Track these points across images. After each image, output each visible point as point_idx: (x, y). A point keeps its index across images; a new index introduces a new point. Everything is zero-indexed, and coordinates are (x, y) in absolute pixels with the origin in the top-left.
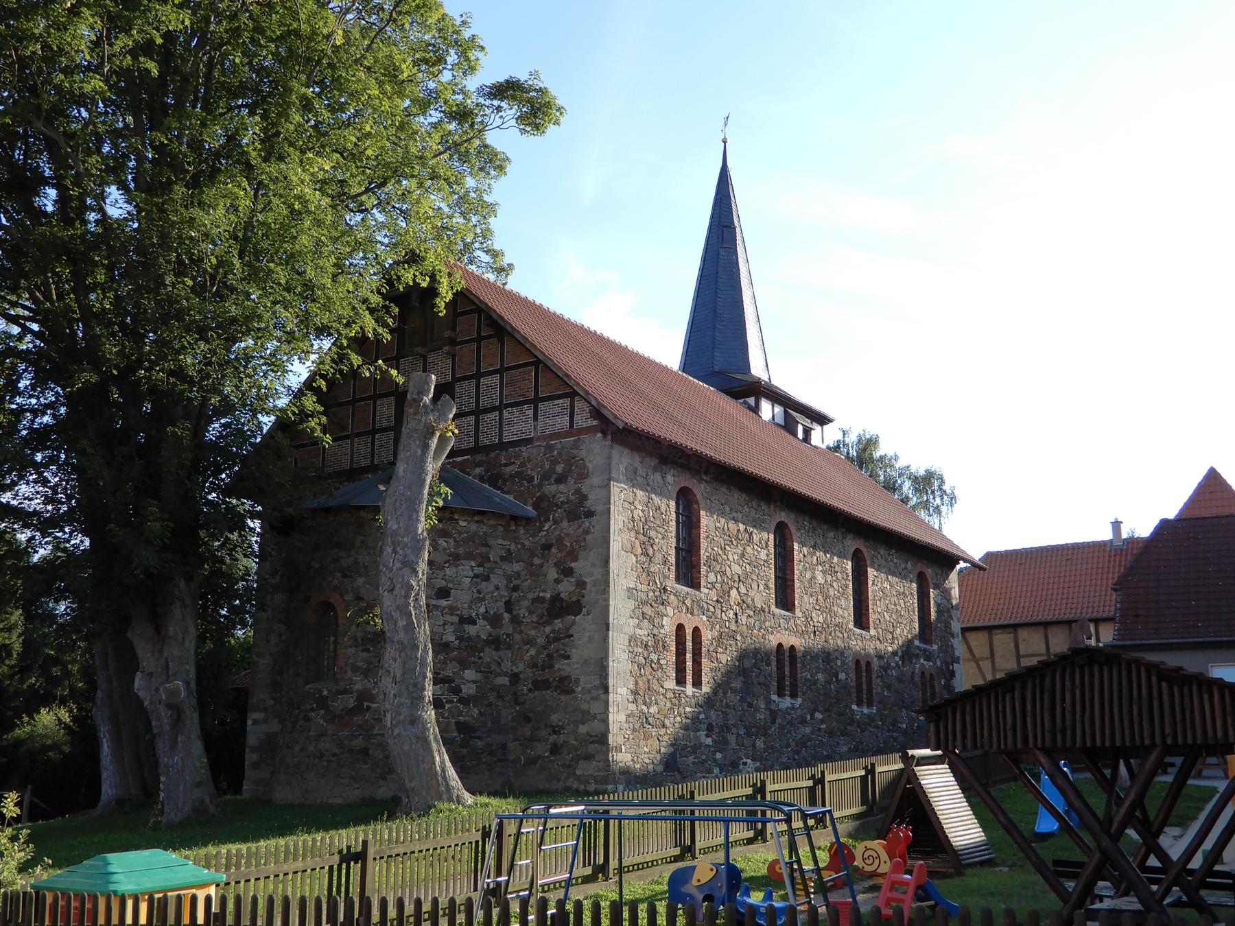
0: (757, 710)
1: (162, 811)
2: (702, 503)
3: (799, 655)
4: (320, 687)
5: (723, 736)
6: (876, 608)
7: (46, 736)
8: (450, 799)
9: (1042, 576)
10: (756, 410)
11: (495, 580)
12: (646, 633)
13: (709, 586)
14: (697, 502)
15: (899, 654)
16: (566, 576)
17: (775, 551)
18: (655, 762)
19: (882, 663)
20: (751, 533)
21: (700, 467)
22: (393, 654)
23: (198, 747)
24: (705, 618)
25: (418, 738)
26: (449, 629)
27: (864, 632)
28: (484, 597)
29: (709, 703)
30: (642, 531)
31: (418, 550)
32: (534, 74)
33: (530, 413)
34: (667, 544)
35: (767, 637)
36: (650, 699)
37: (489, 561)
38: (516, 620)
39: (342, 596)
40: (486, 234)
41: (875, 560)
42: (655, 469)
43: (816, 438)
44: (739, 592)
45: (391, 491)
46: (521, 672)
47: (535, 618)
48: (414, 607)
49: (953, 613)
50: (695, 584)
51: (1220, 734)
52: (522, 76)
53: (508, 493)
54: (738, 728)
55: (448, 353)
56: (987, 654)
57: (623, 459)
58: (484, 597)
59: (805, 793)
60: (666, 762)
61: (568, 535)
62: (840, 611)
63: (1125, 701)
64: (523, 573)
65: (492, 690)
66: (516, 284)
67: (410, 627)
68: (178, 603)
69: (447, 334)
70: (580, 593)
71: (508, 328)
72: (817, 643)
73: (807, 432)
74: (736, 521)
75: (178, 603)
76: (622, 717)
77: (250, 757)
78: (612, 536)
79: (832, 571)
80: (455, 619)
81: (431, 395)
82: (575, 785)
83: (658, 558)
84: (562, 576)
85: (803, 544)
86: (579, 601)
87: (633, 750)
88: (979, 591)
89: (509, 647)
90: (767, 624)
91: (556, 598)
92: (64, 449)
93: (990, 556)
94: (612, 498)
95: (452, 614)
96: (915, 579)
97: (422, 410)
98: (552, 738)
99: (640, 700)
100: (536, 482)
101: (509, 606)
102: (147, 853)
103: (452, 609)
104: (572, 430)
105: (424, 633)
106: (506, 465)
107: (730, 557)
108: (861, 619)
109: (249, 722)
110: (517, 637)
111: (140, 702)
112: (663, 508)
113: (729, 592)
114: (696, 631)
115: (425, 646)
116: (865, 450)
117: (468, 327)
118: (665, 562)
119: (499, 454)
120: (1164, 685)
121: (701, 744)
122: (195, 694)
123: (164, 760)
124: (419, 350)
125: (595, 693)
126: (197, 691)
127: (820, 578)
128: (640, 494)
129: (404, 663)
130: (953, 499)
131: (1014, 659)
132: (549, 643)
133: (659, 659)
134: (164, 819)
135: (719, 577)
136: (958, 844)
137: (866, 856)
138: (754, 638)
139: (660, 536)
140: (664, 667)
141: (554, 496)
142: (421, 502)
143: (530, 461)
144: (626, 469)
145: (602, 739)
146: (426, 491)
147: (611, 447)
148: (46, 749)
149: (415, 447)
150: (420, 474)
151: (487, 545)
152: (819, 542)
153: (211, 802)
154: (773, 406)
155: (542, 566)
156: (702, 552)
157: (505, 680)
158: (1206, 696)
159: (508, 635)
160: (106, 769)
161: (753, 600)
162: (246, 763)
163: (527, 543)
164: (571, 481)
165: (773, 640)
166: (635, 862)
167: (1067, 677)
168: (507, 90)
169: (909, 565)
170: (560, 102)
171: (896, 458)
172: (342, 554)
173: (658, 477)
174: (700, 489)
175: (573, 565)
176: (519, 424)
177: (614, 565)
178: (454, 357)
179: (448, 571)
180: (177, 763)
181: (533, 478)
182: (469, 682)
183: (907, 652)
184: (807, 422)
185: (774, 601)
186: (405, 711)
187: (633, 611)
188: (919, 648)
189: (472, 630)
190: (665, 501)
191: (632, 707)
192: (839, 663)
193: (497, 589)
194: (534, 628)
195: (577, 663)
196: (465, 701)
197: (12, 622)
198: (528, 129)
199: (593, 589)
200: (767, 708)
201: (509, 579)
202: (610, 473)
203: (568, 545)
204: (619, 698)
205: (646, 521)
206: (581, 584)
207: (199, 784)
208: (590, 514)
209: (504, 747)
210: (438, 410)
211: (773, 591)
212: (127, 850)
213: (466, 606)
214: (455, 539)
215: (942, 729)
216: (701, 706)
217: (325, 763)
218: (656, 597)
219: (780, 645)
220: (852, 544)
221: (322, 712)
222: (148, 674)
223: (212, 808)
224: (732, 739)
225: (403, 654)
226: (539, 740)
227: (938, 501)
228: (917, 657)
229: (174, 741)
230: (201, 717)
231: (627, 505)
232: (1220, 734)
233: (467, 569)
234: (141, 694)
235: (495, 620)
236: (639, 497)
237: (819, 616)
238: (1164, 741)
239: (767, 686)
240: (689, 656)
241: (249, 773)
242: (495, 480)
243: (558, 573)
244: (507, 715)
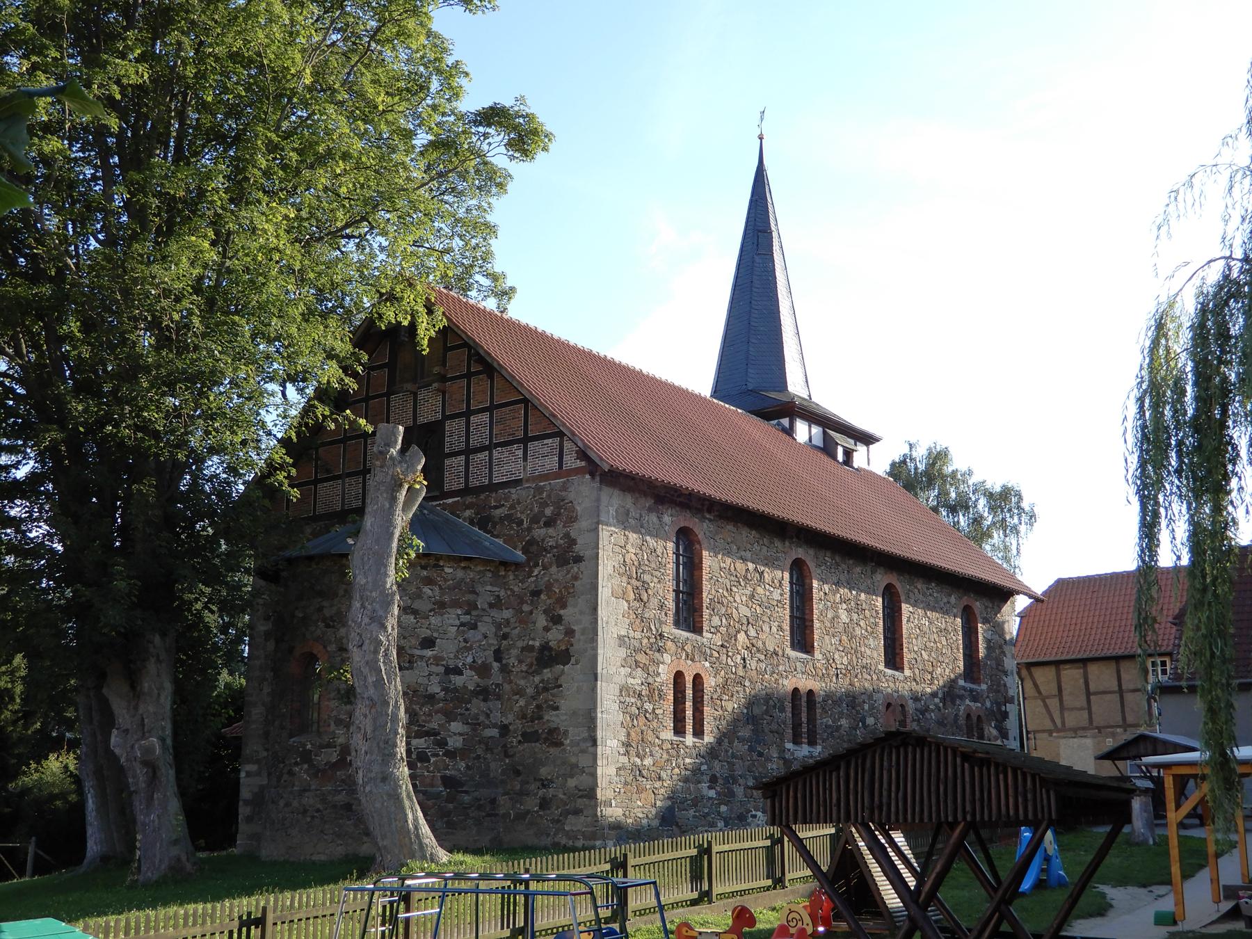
0: (769, 759)
1: (139, 868)
2: (705, 544)
3: (819, 699)
4: (303, 741)
5: (728, 788)
6: (911, 648)
7: (53, 784)
8: (424, 858)
9: (1116, 605)
10: (790, 432)
11: (482, 628)
12: (640, 682)
13: (712, 630)
14: (699, 542)
15: (940, 696)
16: (555, 623)
17: (791, 591)
18: (650, 816)
19: (919, 706)
20: (762, 572)
21: (703, 505)
22: (363, 710)
23: (174, 805)
24: (707, 664)
25: (390, 796)
26: (435, 679)
27: (897, 673)
28: (471, 646)
29: (712, 753)
30: (635, 576)
31: (387, 604)
32: (521, 100)
33: (520, 453)
34: (664, 589)
35: (780, 681)
36: (644, 751)
37: (476, 608)
38: (505, 670)
39: (325, 647)
40: (487, 256)
41: (911, 594)
42: (650, 510)
43: (859, 459)
44: (748, 636)
45: (359, 544)
46: (510, 724)
47: (524, 668)
48: (384, 662)
49: (1007, 649)
50: (697, 629)
51: (1012, 812)
52: (507, 101)
53: (497, 537)
54: (746, 779)
55: (438, 390)
56: (1055, 692)
57: (613, 501)
58: (471, 646)
59: (762, 855)
60: (663, 816)
61: (557, 581)
62: (868, 652)
63: (933, 779)
64: (513, 620)
65: (480, 742)
66: (518, 311)
67: (379, 683)
68: (153, 660)
69: (436, 370)
70: (568, 641)
71: (495, 365)
72: (841, 685)
73: (848, 454)
74: (744, 560)
75: (153, 660)
76: (612, 770)
77: (244, 811)
78: (600, 581)
79: (859, 609)
80: (442, 669)
81: (399, 447)
82: (563, 841)
83: (654, 602)
84: (551, 624)
85: (823, 581)
86: (567, 650)
87: (624, 804)
88: (1047, 623)
89: (499, 697)
90: (781, 668)
91: (545, 647)
92: (56, 494)
93: (1063, 587)
94: (601, 543)
95: (437, 665)
96: (960, 614)
97: (389, 463)
98: (541, 793)
99: (633, 752)
100: (525, 525)
101: (498, 655)
102: (38, 921)
103: (437, 660)
104: (561, 472)
105: (395, 687)
106: (496, 507)
107: (737, 599)
108: (893, 657)
109: (243, 774)
110: (507, 687)
111: (116, 759)
112: (659, 552)
113: (736, 636)
114: (697, 679)
115: (396, 702)
116: (934, 464)
117: (457, 361)
118: (661, 607)
119: (488, 496)
120: (966, 765)
121: (703, 797)
122: (171, 751)
123: (141, 818)
124: (409, 386)
125: (583, 745)
126: (174, 748)
127: (844, 617)
128: (633, 536)
129: (375, 720)
130: (1032, 517)
131: (1084, 698)
132: (538, 693)
133: (654, 709)
134: (141, 878)
135: (724, 621)
136: (894, 906)
137: (790, 918)
138: (765, 684)
139: (656, 580)
140: (660, 716)
141: (543, 540)
142: (389, 556)
143: (519, 503)
144: (616, 511)
145: (590, 793)
146: (395, 545)
147: (600, 489)
148: (53, 797)
149: (383, 501)
150: (388, 527)
151: (474, 592)
152: (842, 578)
153: (188, 860)
154: (810, 426)
155: (531, 613)
156: (704, 595)
157: (494, 732)
158: (1001, 776)
159: (498, 685)
160: (91, 825)
161: (764, 643)
162: (240, 817)
163: (516, 589)
164: (560, 524)
165: (788, 684)
166: (558, 925)
167: (885, 758)
168: (493, 116)
169: (953, 600)
170: (548, 127)
171: (970, 473)
172: (325, 604)
173: (653, 518)
174: (702, 528)
175: (562, 612)
176: (509, 464)
177: (603, 612)
178: (444, 393)
179: (433, 620)
180: (153, 821)
181: (523, 521)
182: (455, 734)
183: (950, 693)
184: (850, 443)
185: (789, 644)
186: (376, 768)
187: (625, 659)
188: (964, 688)
189: (458, 681)
190: (661, 543)
191: (624, 759)
192: (866, 707)
193: (486, 637)
194: (524, 678)
195: (566, 714)
196: (451, 754)
197: (15, 664)
198: (517, 155)
199: (582, 637)
200: (782, 758)
201: (498, 626)
202: (598, 516)
203: (557, 591)
204: (608, 751)
205: (640, 564)
206: (570, 633)
207: (175, 842)
208: (578, 559)
209: (493, 801)
210: (406, 462)
211: (788, 633)
212: (20, 919)
213: (452, 656)
214: (440, 586)
215: (777, 805)
216: (703, 757)
217: (309, 819)
218: (651, 644)
219: (796, 690)
220: (882, 578)
221: (306, 766)
222: (124, 731)
223: (189, 866)
224: (739, 791)
225: (373, 711)
226: (527, 795)
227: (1016, 520)
228: (962, 698)
229: (150, 799)
230: (179, 772)
231: (617, 549)
232: (1012, 812)
233: (452, 618)
234: (117, 751)
235: (483, 670)
236: (631, 540)
237: (842, 657)
238: (964, 818)
239: (781, 735)
240: (689, 704)
241: (243, 827)
242: (484, 523)
243: (547, 620)
244: (496, 768)
